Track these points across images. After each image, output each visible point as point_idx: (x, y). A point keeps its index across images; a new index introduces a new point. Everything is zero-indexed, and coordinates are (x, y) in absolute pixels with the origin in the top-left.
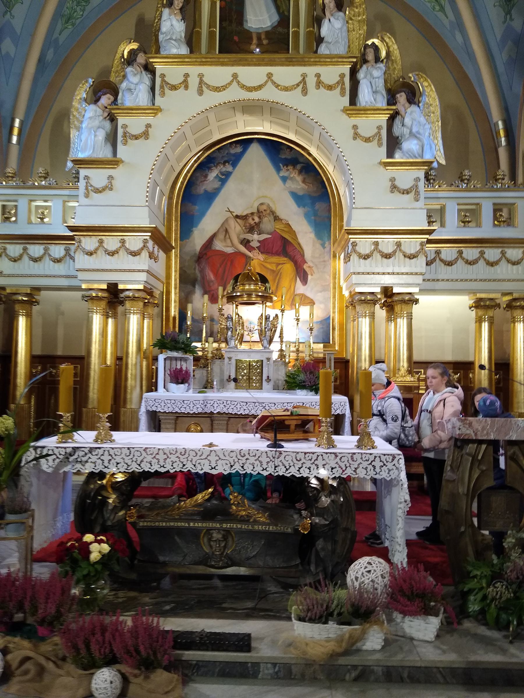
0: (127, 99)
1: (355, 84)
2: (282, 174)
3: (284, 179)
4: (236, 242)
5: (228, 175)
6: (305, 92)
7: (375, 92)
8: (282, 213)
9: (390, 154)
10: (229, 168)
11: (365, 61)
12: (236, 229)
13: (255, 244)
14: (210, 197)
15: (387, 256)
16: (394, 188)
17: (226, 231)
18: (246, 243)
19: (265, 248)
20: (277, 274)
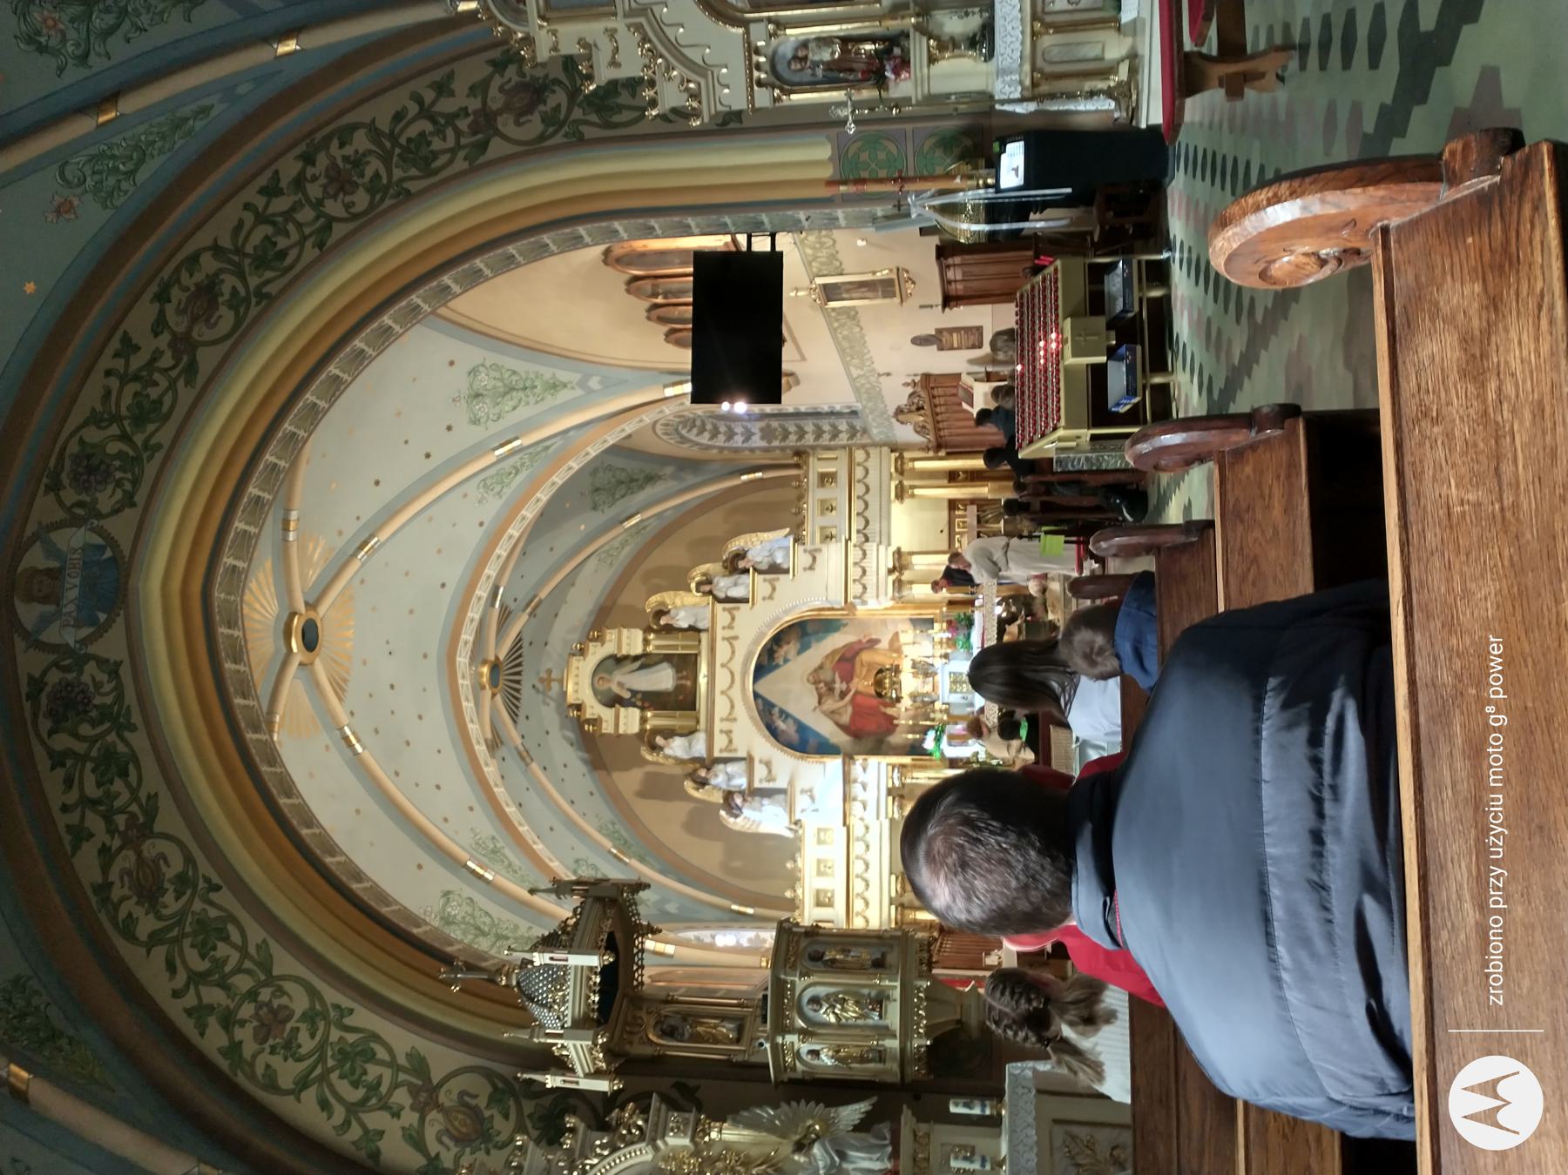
0: (741, 782)
1: (728, 600)
2: (781, 662)
3: (786, 661)
4: (842, 703)
5: (782, 712)
6: (736, 638)
7: (736, 584)
8: (816, 663)
9: (787, 571)
10: (776, 711)
11: (710, 593)
12: (830, 704)
13: (844, 686)
14: (802, 728)
15: (864, 572)
16: (811, 568)
17: (833, 712)
18: (843, 695)
19: (848, 678)
20: (870, 665)
